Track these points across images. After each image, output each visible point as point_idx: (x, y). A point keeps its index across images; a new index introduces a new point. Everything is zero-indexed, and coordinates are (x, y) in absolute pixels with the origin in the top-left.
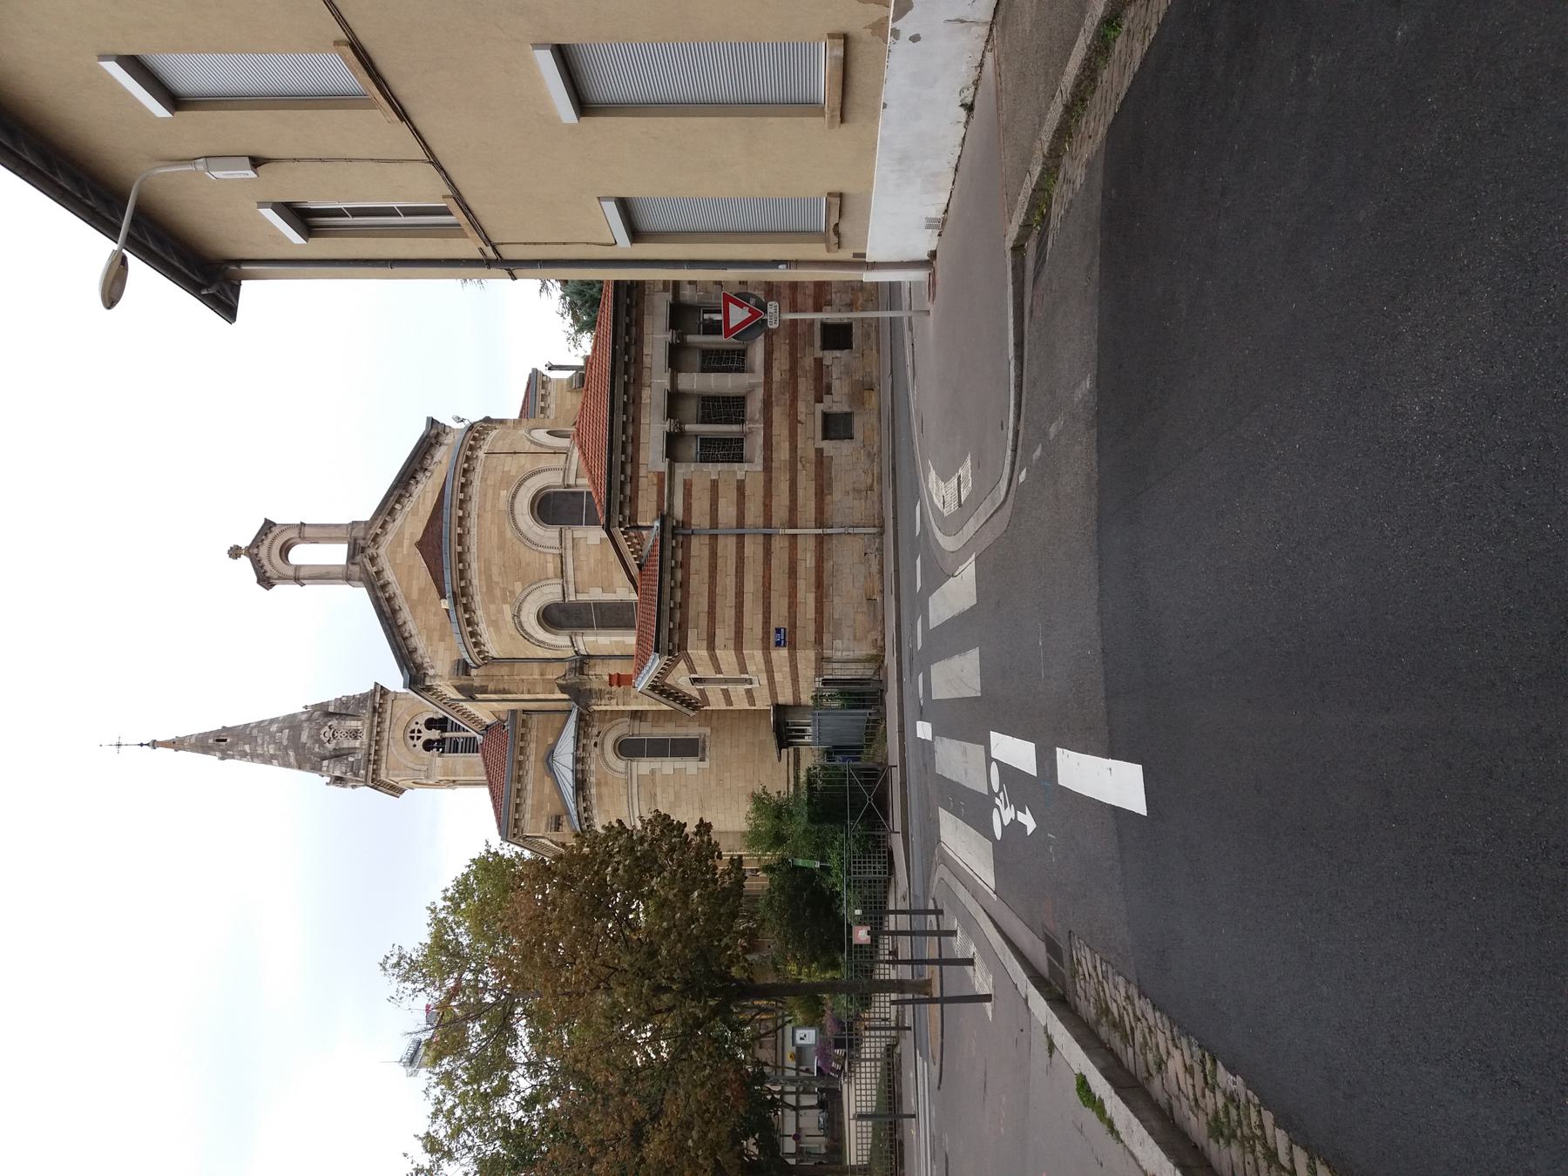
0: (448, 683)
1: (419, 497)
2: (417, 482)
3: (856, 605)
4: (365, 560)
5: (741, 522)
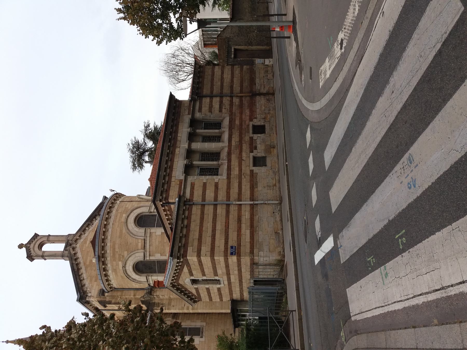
0: (96, 299)
1: (96, 225)
2: (96, 220)
3: (270, 235)
4: (70, 248)
5: (216, 199)
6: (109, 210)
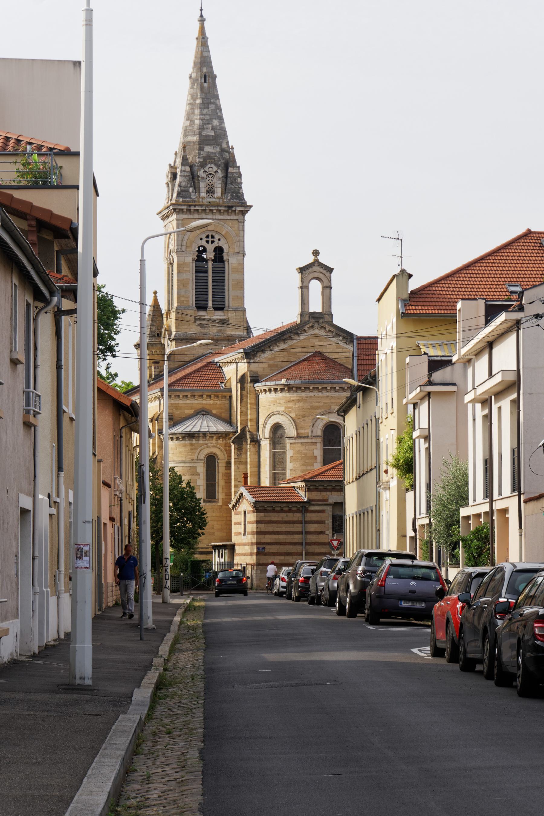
1: (346, 348)
6: (346, 388)
